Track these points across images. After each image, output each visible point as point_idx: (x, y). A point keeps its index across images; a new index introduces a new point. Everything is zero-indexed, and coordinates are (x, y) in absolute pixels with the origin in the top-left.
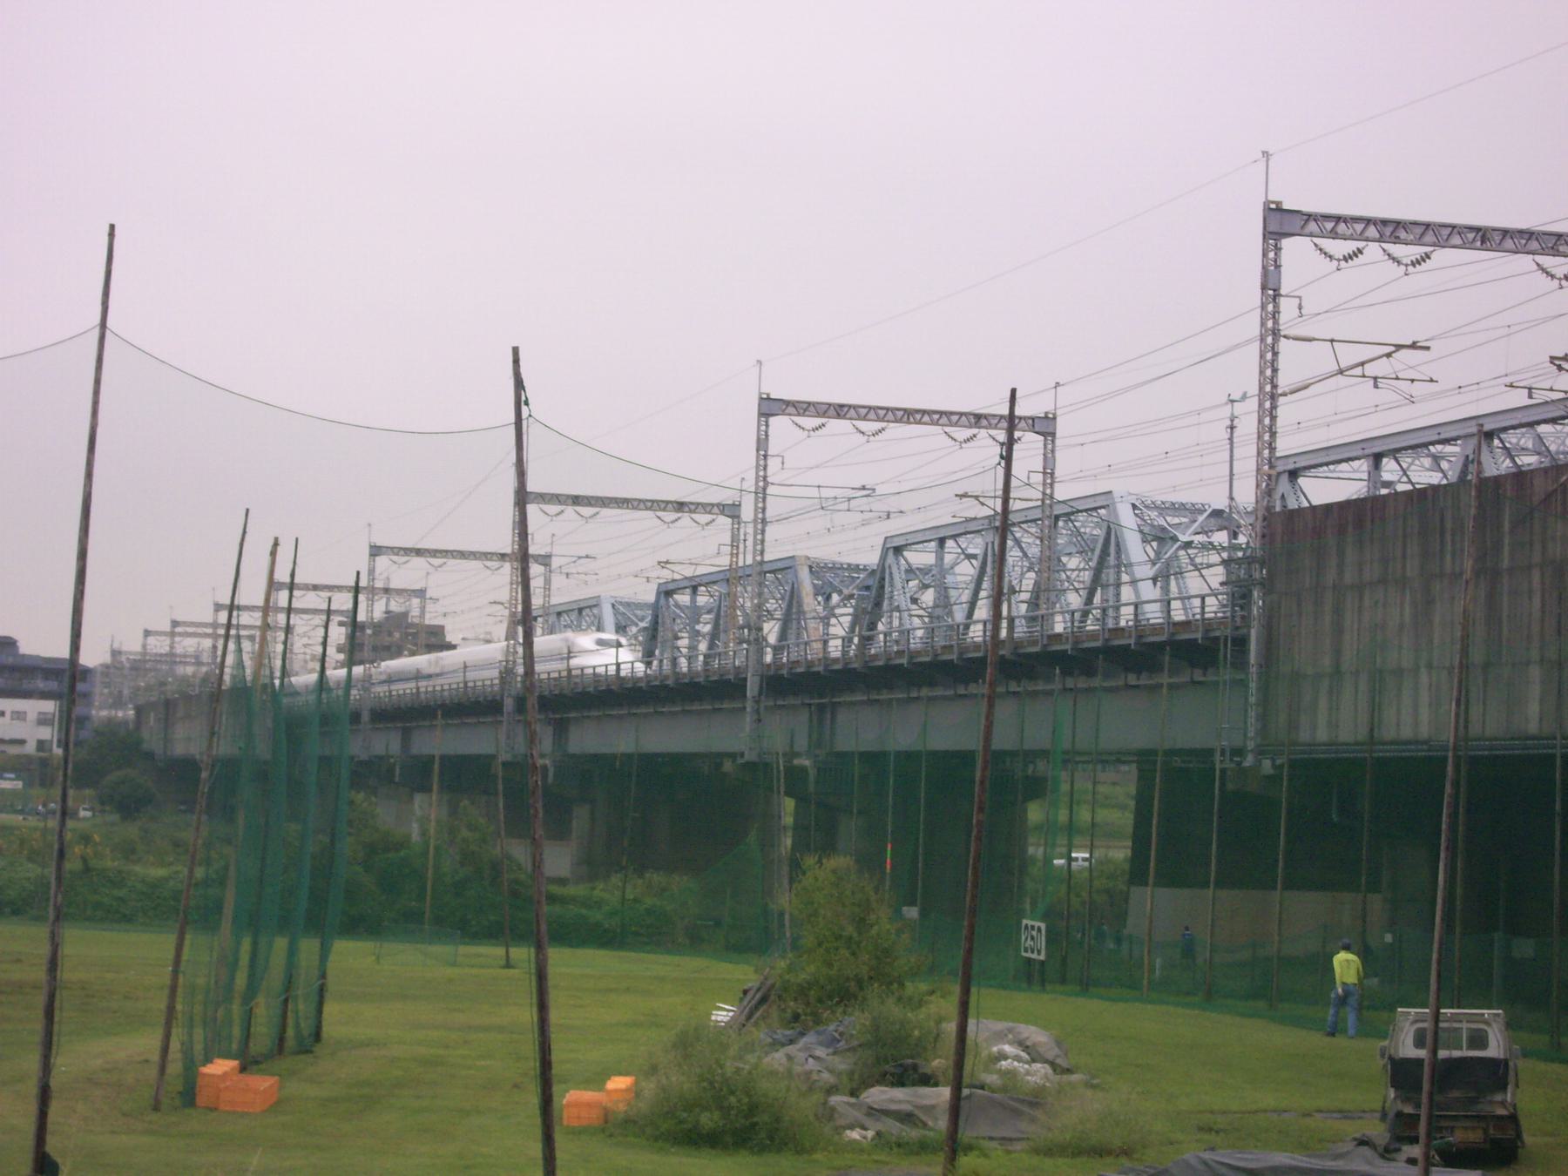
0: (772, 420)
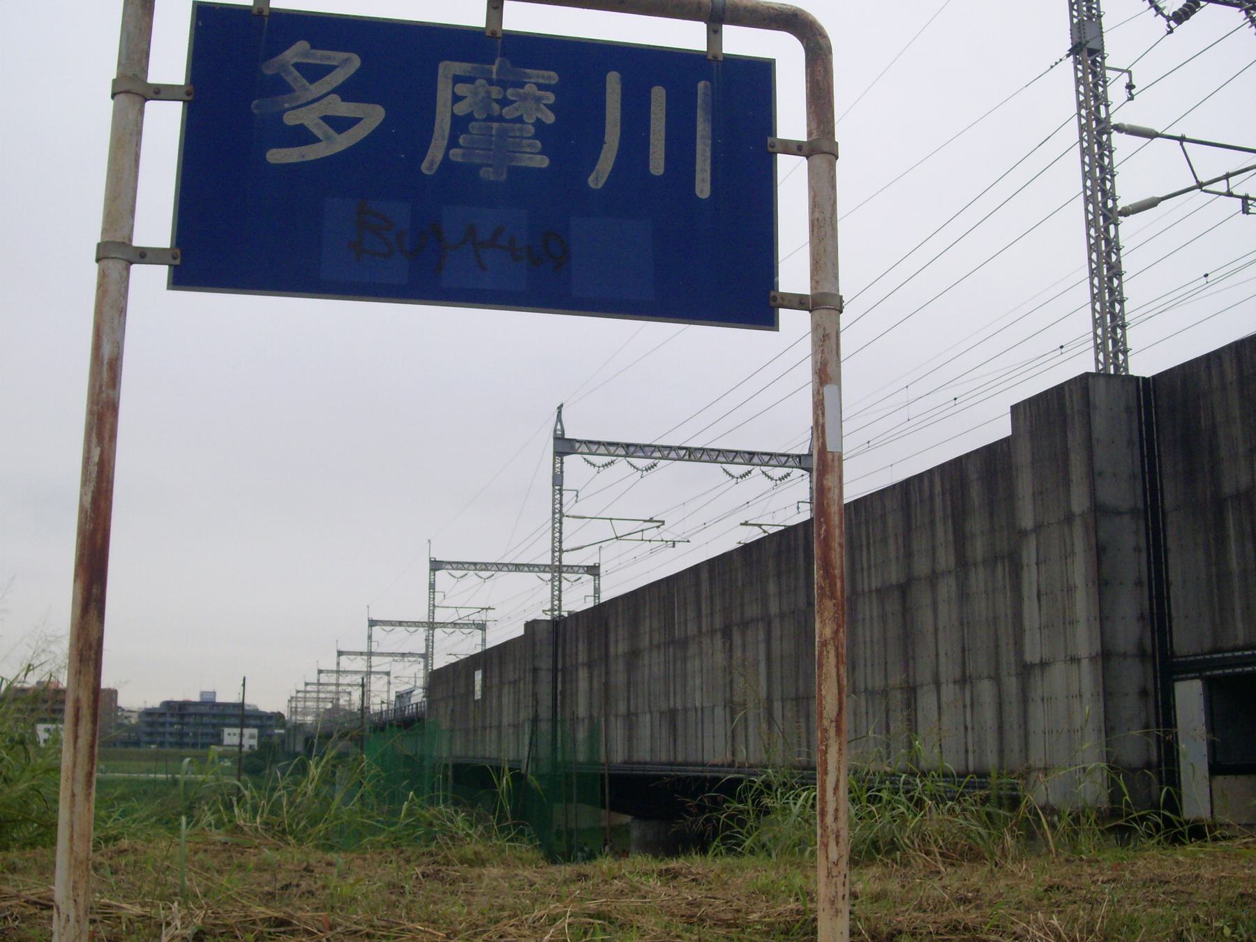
0: (566, 458)
